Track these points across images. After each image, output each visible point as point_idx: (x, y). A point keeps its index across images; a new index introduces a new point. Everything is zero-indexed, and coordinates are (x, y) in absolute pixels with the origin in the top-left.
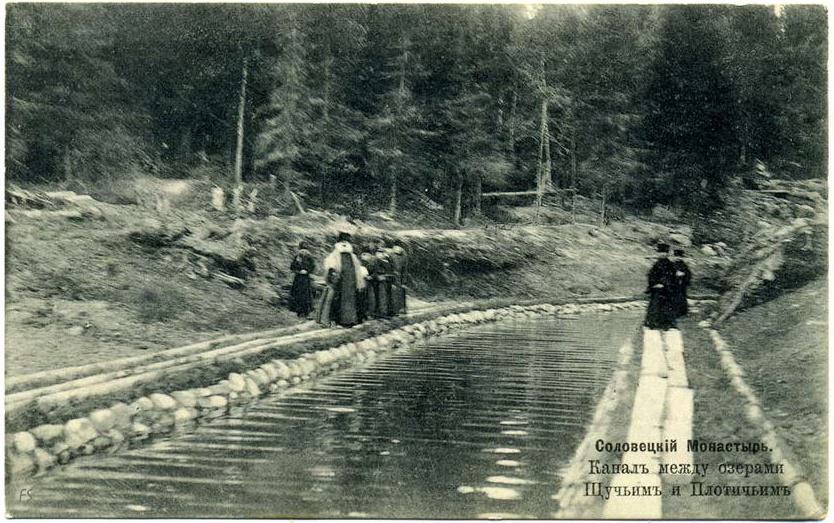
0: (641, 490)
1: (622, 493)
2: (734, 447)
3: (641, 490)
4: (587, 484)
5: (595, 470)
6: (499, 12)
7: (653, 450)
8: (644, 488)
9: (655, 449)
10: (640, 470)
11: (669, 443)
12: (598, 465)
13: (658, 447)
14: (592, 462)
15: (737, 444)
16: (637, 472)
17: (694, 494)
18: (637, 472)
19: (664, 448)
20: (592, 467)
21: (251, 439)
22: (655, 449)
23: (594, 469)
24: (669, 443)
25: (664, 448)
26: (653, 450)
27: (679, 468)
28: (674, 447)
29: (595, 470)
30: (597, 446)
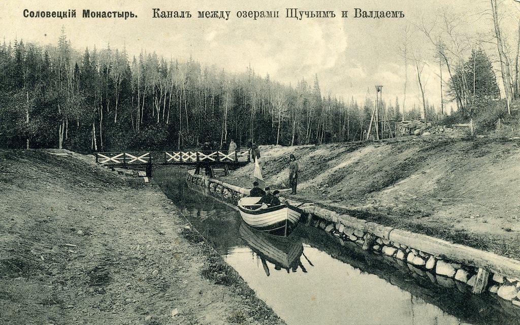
0: (322, 13)
1: (310, 15)
2: (113, 15)
3: (322, 13)
4: (356, 9)
5: (156, 16)
6: (260, 113)
7: (61, 16)
8: (324, 12)
9: (62, 15)
10: (186, 15)
11: (71, 11)
12: (158, 12)
13: (64, 15)
14: (154, 10)
15: (114, 13)
16: (183, 17)
17: (356, 17)
18: (183, 17)
19: (68, 14)
20: (155, 13)
21: (60, 131)
22: (62, 15)
23: (156, 14)
24: (71, 11)
25: (68, 14)
26: (61, 16)
27: (211, 14)
28: (74, 14)
29: (156, 16)
30: (24, 13)
